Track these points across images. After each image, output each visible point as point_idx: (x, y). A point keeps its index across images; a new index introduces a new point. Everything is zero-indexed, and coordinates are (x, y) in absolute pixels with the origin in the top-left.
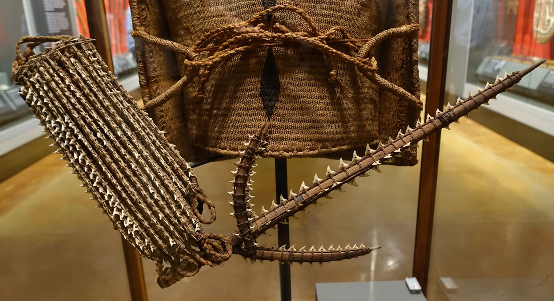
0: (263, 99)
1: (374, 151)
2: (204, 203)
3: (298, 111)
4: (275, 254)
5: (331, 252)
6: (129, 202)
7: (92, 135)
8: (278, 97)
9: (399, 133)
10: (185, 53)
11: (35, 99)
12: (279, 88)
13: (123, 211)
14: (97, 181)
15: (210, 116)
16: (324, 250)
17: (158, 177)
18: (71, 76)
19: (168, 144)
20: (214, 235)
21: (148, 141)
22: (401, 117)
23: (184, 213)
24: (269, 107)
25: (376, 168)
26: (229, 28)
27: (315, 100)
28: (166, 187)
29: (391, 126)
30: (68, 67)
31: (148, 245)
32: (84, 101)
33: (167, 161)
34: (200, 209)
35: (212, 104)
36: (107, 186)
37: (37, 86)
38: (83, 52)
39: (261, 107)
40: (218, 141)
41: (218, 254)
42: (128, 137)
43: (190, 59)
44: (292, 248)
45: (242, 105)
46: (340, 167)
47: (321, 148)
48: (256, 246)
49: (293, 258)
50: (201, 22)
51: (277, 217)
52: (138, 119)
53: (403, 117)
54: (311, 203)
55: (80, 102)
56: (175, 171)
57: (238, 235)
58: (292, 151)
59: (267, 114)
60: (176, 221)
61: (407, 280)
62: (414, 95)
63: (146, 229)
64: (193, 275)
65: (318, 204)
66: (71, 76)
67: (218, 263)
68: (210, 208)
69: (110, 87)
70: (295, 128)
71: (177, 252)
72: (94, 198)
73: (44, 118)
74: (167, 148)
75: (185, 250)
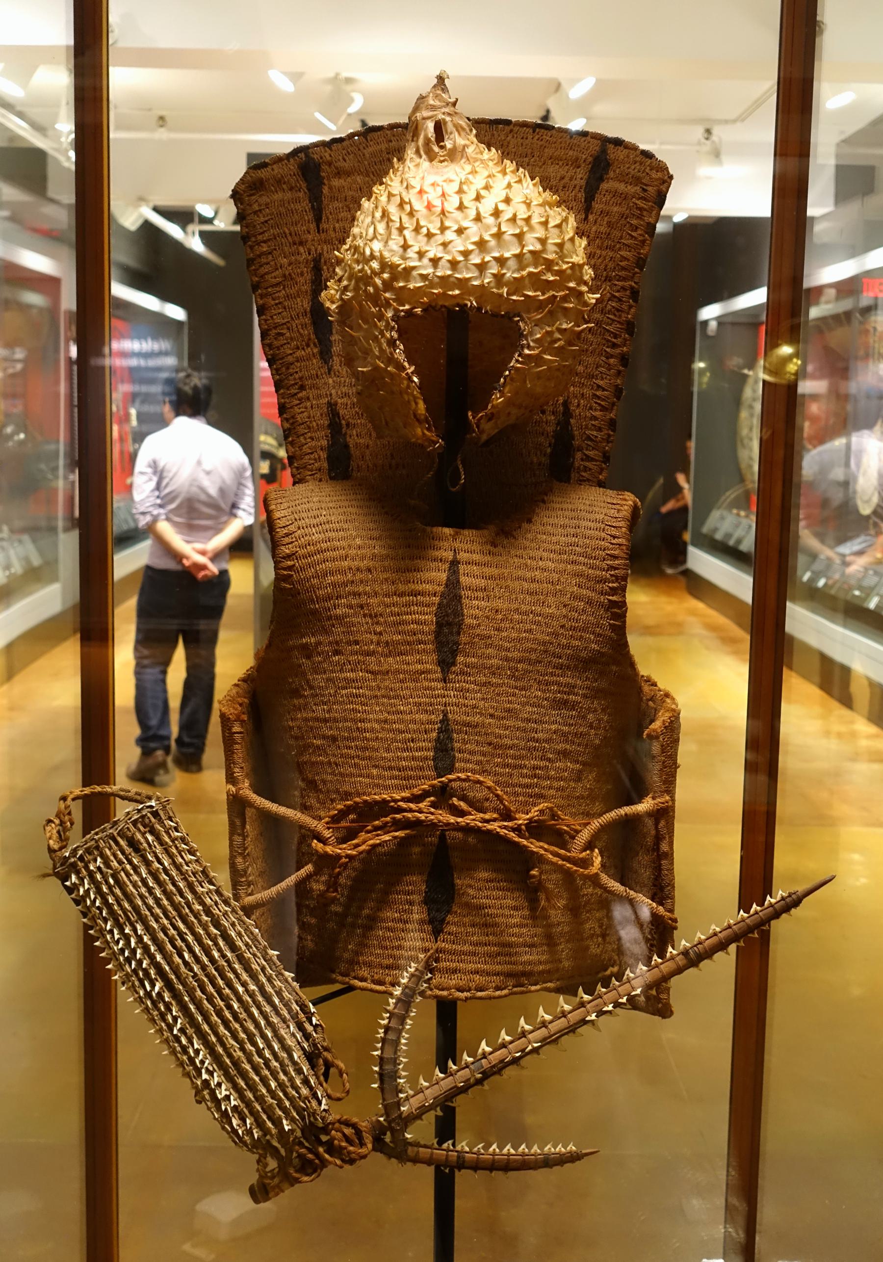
0: (429, 909)
1: (590, 998)
2: (333, 1066)
3: (480, 928)
4: (437, 1154)
5: (523, 1154)
7: (175, 955)
8: (451, 907)
9: (654, 959)
10: (314, 830)
11: (92, 896)
13: (215, 1074)
14: (179, 1026)
16: (512, 1151)
17: (269, 1023)
18: (148, 863)
19: (283, 971)
20: (345, 1117)
21: (255, 966)
23: (306, 1082)
24: (436, 921)
25: (594, 1024)
26: (384, 800)
27: (507, 912)
28: (281, 1040)
30: (145, 850)
33: (282, 999)
34: (326, 1075)
35: (347, 907)
36: (194, 1035)
37: (99, 876)
38: (161, 821)
39: (425, 920)
40: (354, 967)
41: (351, 1148)
42: (228, 961)
43: (324, 841)
44: (462, 1146)
45: (396, 915)
46: (539, 1020)
47: (514, 986)
48: (407, 1138)
49: (464, 1161)
50: (338, 780)
51: (441, 1095)
52: (240, 931)
54: (494, 1073)
55: (160, 904)
57: (382, 1119)
58: (469, 990)
59: (433, 931)
62: (662, 904)
63: (248, 1104)
64: (311, 1181)
66: (148, 863)
67: (352, 1162)
68: (341, 1075)
69: (200, 879)
70: (474, 954)
71: (292, 1141)
72: (170, 1052)
73: (103, 926)
74: (280, 977)
75: (302, 1139)
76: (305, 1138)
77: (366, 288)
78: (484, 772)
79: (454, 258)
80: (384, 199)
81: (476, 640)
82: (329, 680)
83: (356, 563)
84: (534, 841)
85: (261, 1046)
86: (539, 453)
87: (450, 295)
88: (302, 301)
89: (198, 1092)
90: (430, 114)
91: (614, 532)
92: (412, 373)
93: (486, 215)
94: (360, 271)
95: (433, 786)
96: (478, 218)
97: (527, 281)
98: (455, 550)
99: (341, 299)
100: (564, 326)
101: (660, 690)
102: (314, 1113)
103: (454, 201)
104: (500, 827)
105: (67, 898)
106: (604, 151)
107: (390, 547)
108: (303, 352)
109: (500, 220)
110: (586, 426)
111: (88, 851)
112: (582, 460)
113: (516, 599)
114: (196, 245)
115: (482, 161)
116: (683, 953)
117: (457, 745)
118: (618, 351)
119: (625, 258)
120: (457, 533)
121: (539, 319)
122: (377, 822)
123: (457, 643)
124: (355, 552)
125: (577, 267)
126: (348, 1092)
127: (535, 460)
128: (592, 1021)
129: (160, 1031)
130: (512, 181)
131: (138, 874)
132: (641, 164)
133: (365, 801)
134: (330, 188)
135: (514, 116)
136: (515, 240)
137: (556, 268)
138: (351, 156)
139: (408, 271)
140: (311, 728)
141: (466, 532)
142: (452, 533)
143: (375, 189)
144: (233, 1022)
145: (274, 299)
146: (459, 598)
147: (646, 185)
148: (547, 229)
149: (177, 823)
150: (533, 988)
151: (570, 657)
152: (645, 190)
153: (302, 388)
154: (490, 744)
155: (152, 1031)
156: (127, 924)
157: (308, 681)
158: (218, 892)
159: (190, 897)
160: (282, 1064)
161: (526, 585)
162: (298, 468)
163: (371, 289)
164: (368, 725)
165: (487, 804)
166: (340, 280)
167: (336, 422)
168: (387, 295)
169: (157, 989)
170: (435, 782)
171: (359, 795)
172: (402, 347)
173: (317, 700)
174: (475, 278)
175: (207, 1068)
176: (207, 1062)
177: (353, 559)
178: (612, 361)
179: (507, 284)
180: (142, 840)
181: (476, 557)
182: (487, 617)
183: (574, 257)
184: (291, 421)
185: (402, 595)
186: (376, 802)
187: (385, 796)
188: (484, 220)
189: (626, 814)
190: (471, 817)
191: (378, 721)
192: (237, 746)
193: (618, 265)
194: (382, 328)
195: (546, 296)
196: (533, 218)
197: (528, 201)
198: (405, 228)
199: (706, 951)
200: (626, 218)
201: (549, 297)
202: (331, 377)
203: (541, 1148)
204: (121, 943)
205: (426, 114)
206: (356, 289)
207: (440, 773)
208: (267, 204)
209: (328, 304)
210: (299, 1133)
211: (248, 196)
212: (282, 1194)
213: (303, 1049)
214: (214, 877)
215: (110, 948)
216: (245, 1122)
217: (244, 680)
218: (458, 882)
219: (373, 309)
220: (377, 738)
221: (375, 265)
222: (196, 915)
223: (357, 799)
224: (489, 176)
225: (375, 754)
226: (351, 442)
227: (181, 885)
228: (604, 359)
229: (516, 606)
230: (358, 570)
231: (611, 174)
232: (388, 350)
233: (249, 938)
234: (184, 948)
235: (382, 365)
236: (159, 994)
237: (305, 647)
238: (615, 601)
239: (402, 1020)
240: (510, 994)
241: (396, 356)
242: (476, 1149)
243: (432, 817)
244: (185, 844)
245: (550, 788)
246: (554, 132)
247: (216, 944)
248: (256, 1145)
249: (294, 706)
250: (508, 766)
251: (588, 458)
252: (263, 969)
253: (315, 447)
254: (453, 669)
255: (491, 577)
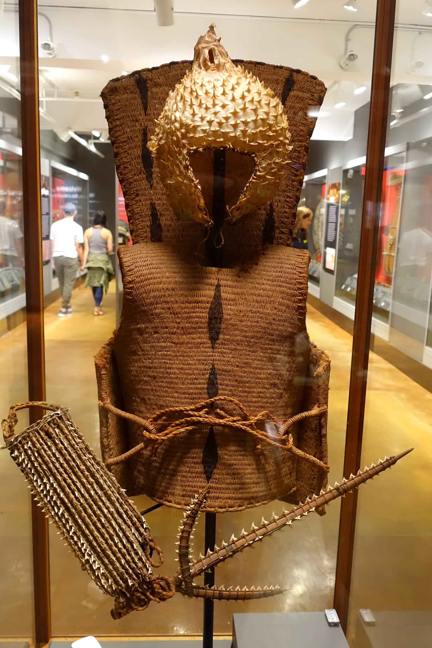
0: (204, 466)
2: (154, 549)
4: (209, 592)
6: (99, 549)
7: (71, 494)
11: (26, 462)
12: (217, 458)
13: (92, 556)
15: (159, 473)
16: (247, 590)
17: (121, 528)
18: (56, 445)
20: (161, 576)
21: (113, 498)
22: (315, 471)
23: (140, 559)
26: (181, 411)
28: (127, 538)
29: (307, 476)
30: (54, 437)
31: (111, 584)
32: (65, 465)
33: (127, 515)
34: (151, 554)
35: (161, 464)
36: (81, 536)
37: (29, 452)
38: (63, 421)
41: (164, 593)
42: (99, 496)
43: (149, 431)
46: (262, 524)
47: (248, 504)
49: (222, 596)
53: (316, 472)
56: (134, 524)
57: (180, 576)
58: (225, 508)
59: (206, 478)
60: (134, 565)
61: (327, 611)
63: (110, 572)
65: (244, 552)
66: (56, 445)
68: (159, 554)
69: (84, 452)
70: (228, 489)
72: (68, 544)
73: (32, 478)
74: (127, 503)
75: (138, 588)
76: (140, 588)
77: (172, 138)
78: (233, 395)
79: (220, 121)
80: (181, 90)
81: (230, 326)
82: (152, 347)
83: (166, 286)
84: (259, 431)
85: (117, 541)
86: (257, 230)
87: (218, 141)
88: (137, 151)
89: (83, 565)
90: (206, 45)
91: (301, 270)
92: (197, 183)
93: (238, 98)
94: (169, 129)
95: (207, 403)
96: (233, 100)
97: (259, 135)
98: (218, 279)
99: (159, 144)
100: (277, 161)
101: (318, 350)
102: (145, 576)
103: (220, 90)
104: (241, 424)
105: (14, 463)
106: (291, 76)
107: (184, 277)
108: (138, 177)
109: (245, 101)
110: (281, 216)
111: (24, 438)
112: (279, 233)
113: (250, 305)
114: (93, 149)
115: (234, 71)
116: (336, 489)
117: (219, 381)
118: (298, 178)
119: (302, 130)
120: (219, 270)
121: (264, 157)
122: (177, 422)
123: (220, 328)
124: (165, 280)
125: (284, 130)
126: (162, 563)
127: (255, 233)
128: (289, 525)
129: (63, 533)
130: (251, 81)
131: (51, 450)
132: (311, 82)
133: (171, 411)
134: (152, 93)
135: (245, 60)
136: (253, 112)
137: (274, 129)
138: (162, 77)
139: (195, 128)
140: (143, 371)
141: (224, 270)
142: (217, 270)
143: (176, 85)
144: (102, 529)
145: (123, 149)
146: (220, 305)
147: (313, 93)
148: (269, 107)
149: (72, 422)
150: (257, 504)
151: (279, 335)
152: (312, 96)
153: (137, 195)
154: (236, 381)
155: (59, 533)
156: (45, 477)
157: (141, 347)
158: (94, 459)
159: (78, 462)
160: (128, 551)
161: (255, 298)
162: (135, 236)
163: (175, 138)
164: (172, 371)
165: (235, 412)
166: (158, 135)
167: (155, 213)
168: (184, 141)
169: (61, 511)
170: (208, 401)
171: (168, 407)
172: (192, 169)
173: (145, 357)
174: (232, 132)
175: (88, 553)
176: (88, 550)
177: (164, 284)
178: (295, 183)
179: (249, 136)
180: (53, 432)
181: (229, 283)
182: (235, 315)
183: (282, 124)
184: (132, 212)
185: (190, 303)
186: (176, 411)
187: (181, 408)
188: (236, 101)
189: (306, 416)
190: (227, 419)
191: (178, 369)
192: (104, 381)
193: (299, 134)
194: (181, 159)
195: (269, 144)
196: (262, 101)
197: (259, 92)
198: (193, 105)
199: (348, 488)
200: (303, 110)
201: (270, 144)
202: (152, 190)
203: (262, 587)
204: (42, 487)
205: (204, 45)
206: (167, 138)
207: (210, 396)
208: (119, 100)
209: (151, 149)
210: (137, 585)
211: (109, 95)
212: (128, 615)
213: (139, 541)
214: (91, 450)
215: (36, 489)
216: (108, 581)
217: (108, 345)
218: (219, 452)
219: (176, 149)
220: (177, 377)
221: (177, 125)
222: (82, 472)
223: (167, 409)
224: (239, 78)
225: (176, 386)
226: (162, 224)
227: (74, 456)
228: (291, 182)
229: (250, 309)
230: (167, 289)
231: (295, 87)
232: (184, 171)
233: (110, 482)
234: (76, 489)
235: (181, 180)
236: (63, 514)
237: (139, 329)
238: (301, 306)
239: (191, 526)
240: (246, 508)
241: (188, 174)
242: (228, 589)
243: (207, 420)
244: (76, 433)
245: (267, 403)
246: (265, 66)
247: (93, 487)
248: (114, 593)
249: (134, 359)
250: (246, 392)
251: (283, 233)
252: (118, 499)
253: (144, 226)
254: (218, 342)
255: (237, 294)
